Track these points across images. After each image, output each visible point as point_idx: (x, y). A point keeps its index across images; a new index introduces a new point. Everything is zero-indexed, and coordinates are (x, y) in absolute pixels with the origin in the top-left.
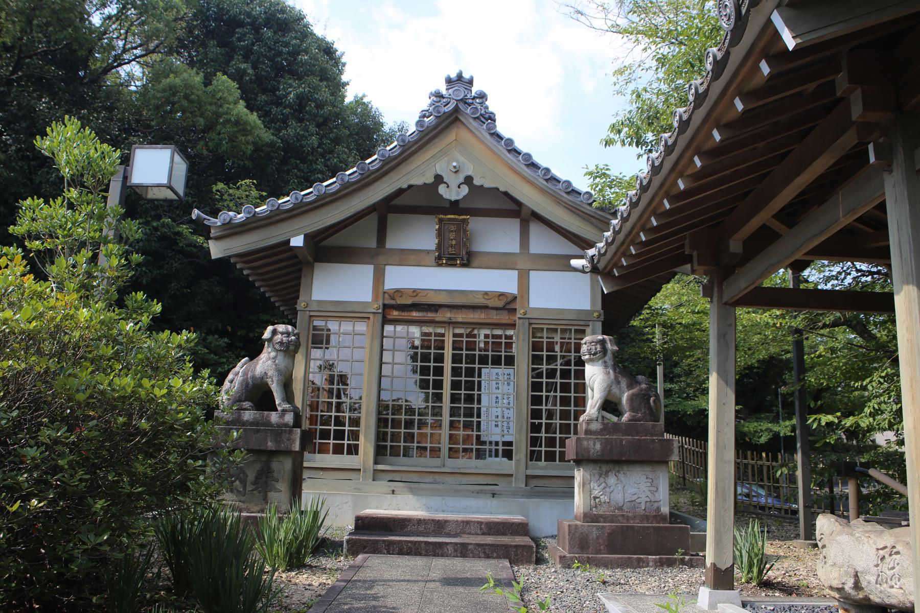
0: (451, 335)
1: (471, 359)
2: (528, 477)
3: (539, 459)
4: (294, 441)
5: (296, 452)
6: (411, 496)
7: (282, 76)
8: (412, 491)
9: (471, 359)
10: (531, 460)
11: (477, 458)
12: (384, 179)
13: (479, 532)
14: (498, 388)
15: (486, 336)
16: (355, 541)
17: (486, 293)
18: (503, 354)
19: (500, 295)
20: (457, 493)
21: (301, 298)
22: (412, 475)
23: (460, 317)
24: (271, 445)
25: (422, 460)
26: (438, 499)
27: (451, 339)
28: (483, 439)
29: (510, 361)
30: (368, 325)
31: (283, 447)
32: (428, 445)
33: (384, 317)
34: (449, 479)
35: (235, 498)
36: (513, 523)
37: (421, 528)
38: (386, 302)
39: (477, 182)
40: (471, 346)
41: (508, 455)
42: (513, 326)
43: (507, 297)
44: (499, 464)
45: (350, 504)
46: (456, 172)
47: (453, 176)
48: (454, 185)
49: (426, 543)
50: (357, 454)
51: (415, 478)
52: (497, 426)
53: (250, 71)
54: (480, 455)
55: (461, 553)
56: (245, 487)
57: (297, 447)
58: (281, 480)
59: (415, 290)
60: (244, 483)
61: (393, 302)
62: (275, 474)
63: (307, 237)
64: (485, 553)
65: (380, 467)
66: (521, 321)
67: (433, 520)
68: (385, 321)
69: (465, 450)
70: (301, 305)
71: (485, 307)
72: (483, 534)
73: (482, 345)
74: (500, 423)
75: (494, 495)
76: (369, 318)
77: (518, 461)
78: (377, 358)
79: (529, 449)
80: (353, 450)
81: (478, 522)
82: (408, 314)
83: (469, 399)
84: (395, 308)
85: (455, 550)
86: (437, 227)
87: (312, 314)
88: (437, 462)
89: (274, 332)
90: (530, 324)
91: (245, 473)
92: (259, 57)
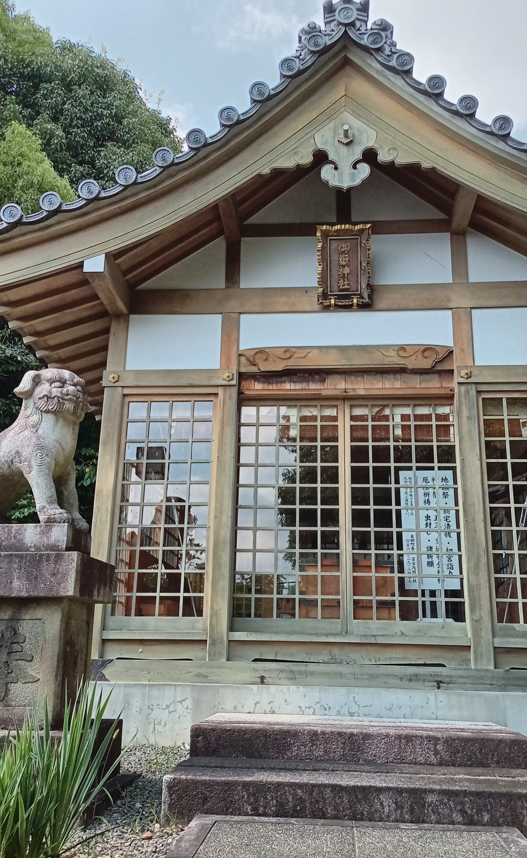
0: (348, 417)
1: (381, 454)
2: (499, 652)
3: (513, 618)
4: (65, 575)
5: (70, 599)
6: (293, 688)
7: (103, 146)
8: (293, 678)
9: (381, 454)
10: (500, 620)
11: (403, 618)
12: (232, 163)
13: (433, 759)
14: (428, 502)
15: (405, 418)
17: (402, 348)
18: (435, 444)
19: (425, 350)
20: (373, 680)
21: (109, 367)
22: (294, 649)
23: (361, 387)
24: (19, 587)
25: (309, 623)
26: (342, 691)
27: (348, 423)
28: (408, 586)
29: (447, 455)
30: (215, 406)
31: (41, 591)
32: (319, 597)
33: (240, 393)
34: (356, 655)
36: (500, 741)
37: (319, 752)
38: (243, 370)
39: (383, 157)
40: (380, 433)
41: (456, 612)
42: (448, 398)
43: (437, 353)
44: (438, 628)
45: (188, 703)
46: (347, 144)
47: (344, 150)
48: (345, 166)
49: (335, 788)
51: (300, 655)
52: (430, 564)
53: (60, 132)
54: (408, 612)
55: (412, 811)
57: (70, 588)
59: (287, 350)
61: (254, 369)
62: (27, 646)
63: (112, 257)
64: (463, 812)
65: (239, 636)
66: (463, 388)
67: (340, 734)
68: (243, 400)
69: (381, 604)
70: (108, 377)
71: (402, 371)
72: (441, 763)
73: (399, 432)
74: (435, 560)
75: (439, 684)
76: (216, 394)
77: (476, 622)
78: (230, 455)
79: (495, 600)
80: (193, 608)
81: (430, 739)
82: (279, 386)
83: (383, 518)
84: (258, 379)
85: (399, 806)
86: (320, 245)
87: (126, 391)
88: (336, 625)
89: (37, 381)
90: (479, 392)
92: (72, 120)
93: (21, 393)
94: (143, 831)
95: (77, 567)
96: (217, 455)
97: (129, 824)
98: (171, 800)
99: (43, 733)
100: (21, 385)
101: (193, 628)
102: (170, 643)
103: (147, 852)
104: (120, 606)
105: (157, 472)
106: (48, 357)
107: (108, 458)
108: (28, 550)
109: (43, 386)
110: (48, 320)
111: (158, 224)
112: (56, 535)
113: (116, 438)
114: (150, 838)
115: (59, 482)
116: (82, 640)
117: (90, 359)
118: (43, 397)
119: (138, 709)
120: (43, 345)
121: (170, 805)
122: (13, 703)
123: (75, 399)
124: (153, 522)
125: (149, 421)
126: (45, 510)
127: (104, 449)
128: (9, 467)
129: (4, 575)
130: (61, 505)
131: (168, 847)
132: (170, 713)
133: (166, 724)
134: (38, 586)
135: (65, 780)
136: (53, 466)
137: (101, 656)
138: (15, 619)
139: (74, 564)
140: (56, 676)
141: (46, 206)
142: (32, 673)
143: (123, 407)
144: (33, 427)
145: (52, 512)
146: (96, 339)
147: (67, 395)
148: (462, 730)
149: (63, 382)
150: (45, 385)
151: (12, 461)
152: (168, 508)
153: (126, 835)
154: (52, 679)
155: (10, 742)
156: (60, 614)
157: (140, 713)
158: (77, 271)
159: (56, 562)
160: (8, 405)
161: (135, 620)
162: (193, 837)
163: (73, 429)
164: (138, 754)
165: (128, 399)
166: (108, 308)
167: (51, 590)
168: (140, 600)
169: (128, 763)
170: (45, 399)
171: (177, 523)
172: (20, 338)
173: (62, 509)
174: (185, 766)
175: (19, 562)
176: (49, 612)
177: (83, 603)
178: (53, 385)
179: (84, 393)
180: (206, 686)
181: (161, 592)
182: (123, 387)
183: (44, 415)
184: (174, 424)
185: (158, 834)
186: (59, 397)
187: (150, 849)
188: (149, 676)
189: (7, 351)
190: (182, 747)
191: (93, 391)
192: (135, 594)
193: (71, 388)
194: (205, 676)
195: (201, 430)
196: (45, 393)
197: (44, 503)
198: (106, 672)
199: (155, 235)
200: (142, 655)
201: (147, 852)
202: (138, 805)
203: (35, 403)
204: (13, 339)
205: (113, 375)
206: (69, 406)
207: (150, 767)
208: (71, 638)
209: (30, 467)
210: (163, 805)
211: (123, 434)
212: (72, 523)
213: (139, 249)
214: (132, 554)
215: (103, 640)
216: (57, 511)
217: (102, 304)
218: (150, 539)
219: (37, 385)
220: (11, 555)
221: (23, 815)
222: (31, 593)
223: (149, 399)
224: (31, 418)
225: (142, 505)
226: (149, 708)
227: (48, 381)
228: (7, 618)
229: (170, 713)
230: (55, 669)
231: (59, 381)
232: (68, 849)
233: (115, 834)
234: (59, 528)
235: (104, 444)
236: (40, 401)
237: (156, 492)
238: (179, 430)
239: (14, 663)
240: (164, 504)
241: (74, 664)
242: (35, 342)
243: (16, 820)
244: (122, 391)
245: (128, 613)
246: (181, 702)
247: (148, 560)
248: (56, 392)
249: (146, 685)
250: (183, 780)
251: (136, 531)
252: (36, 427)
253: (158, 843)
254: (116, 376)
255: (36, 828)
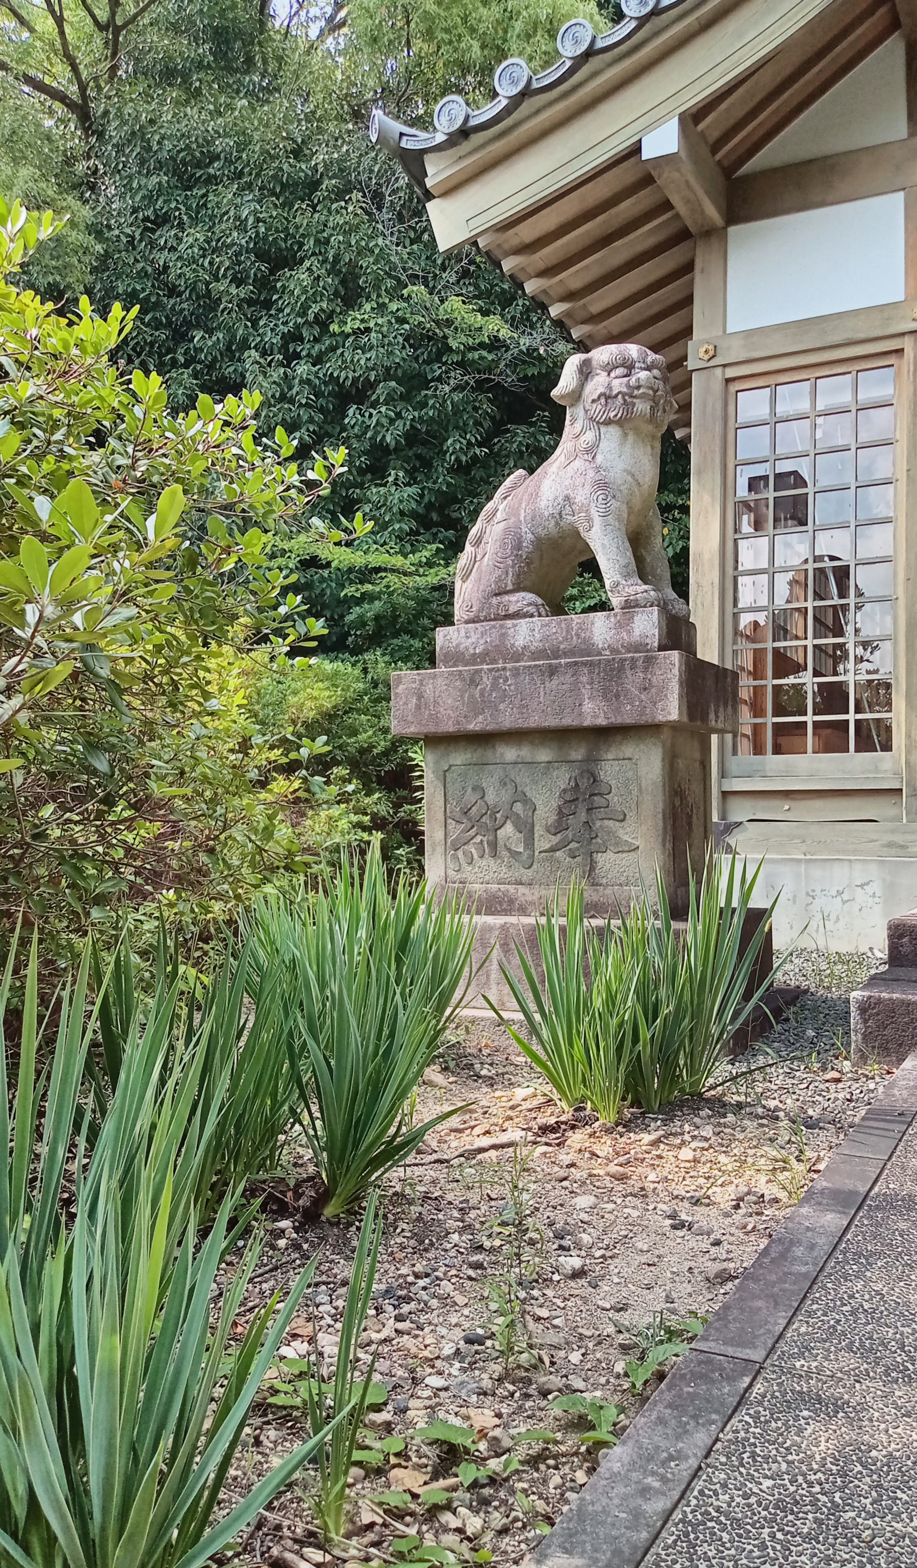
4: (662, 690)
5: (674, 727)
16: (891, 1010)
24: (593, 712)
30: (897, 377)
31: (627, 716)
35: (504, 873)
50: (887, 747)
56: (529, 842)
57: (671, 709)
58: (631, 815)
60: (527, 829)
62: (614, 798)
63: (692, 119)
70: (696, 352)
76: (899, 352)
87: (731, 373)
89: (585, 372)
91: (525, 800)
93: (562, 397)
94: (824, 1069)
95: (681, 675)
96: (905, 468)
97: (801, 1059)
98: (867, 1028)
99: (658, 924)
100: (562, 383)
101: (876, 770)
102: (834, 796)
103: (837, 1099)
104: (745, 741)
105: (795, 512)
106: (590, 336)
107: (707, 498)
108: (599, 654)
109: (596, 378)
110: (586, 267)
111: (773, 33)
112: (642, 627)
113: (718, 460)
114: (838, 1081)
115: (637, 540)
116: (696, 787)
117: (666, 320)
118: (599, 397)
119: (790, 896)
120: (582, 314)
121: (865, 1036)
122: (604, 881)
123: (651, 392)
124: (788, 602)
125: (775, 421)
126: (620, 588)
127: (699, 483)
128: (557, 524)
129: (568, 694)
130: (644, 579)
131: (872, 1095)
132: (844, 902)
133: (838, 919)
134: (623, 709)
135: (701, 987)
136: (625, 515)
137: (723, 817)
138: (592, 760)
139: (676, 671)
140: (664, 840)
141: (569, 50)
142: (626, 838)
143: (728, 401)
144: (587, 451)
145: (631, 590)
146: (677, 283)
147: (638, 388)
148: (137, 1193)
149: (629, 366)
150: (598, 376)
151: (560, 514)
152: (820, 572)
153: (798, 1074)
154: (658, 847)
155: (613, 932)
156: (660, 750)
157: (794, 902)
158: (632, 160)
159: (646, 669)
160: (533, 435)
161: (773, 761)
162: (912, 1083)
163: (653, 448)
164: (796, 961)
165: (733, 387)
166: (689, 224)
167: (642, 713)
168: (779, 729)
169: (785, 974)
170: (603, 401)
171: (836, 598)
172: (544, 307)
173: (646, 583)
174: (883, 979)
175: (589, 673)
176: (642, 747)
177: (693, 733)
178: (613, 375)
179: (665, 380)
180: (904, 862)
181: (815, 714)
182: (724, 366)
183: (603, 429)
184: (820, 420)
185: (849, 1075)
186: (624, 394)
187: (841, 1096)
188: (804, 847)
189: (522, 341)
190: (869, 954)
191: (677, 379)
192: (771, 720)
193: (643, 375)
194: (902, 847)
195: (879, 423)
196: (601, 390)
197: (617, 578)
198: (731, 841)
199: (767, 58)
200: (788, 813)
201: (837, 1099)
202: (811, 1033)
203: (586, 411)
204: (528, 319)
205: (706, 346)
206: (642, 407)
207: (821, 980)
208: (679, 786)
209: (589, 520)
210: (852, 1033)
211: (730, 452)
212: (663, 606)
213: (741, 90)
214: (759, 655)
215: (723, 792)
216: (638, 589)
217: (677, 215)
218: (786, 631)
219: (586, 379)
220: (576, 663)
221: (645, 1034)
222: (613, 720)
223: (772, 380)
224: (582, 438)
225: (771, 572)
226: (808, 894)
227: (603, 368)
228: (580, 758)
229: (844, 902)
230: (660, 832)
231: (622, 365)
232: (712, 1088)
233: (781, 1071)
234: (645, 617)
235: (699, 473)
236: (594, 405)
237: (794, 549)
238: (836, 431)
239: (598, 823)
240: (810, 566)
241: (688, 828)
242: (568, 314)
243: (636, 1040)
244: (724, 373)
245: (758, 750)
246: (862, 886)
247: (785, 664)
248: (618, 385)
249: (801, 860)
250: (885, 1000)
251: (761, 618)
252: (591, 451)
253: (853, 1088)
254: (711, 347)
255: (665, 1053)
